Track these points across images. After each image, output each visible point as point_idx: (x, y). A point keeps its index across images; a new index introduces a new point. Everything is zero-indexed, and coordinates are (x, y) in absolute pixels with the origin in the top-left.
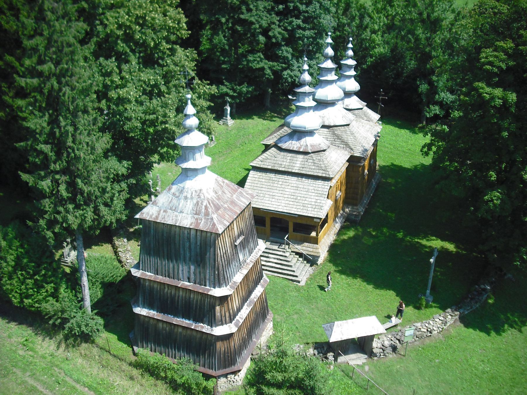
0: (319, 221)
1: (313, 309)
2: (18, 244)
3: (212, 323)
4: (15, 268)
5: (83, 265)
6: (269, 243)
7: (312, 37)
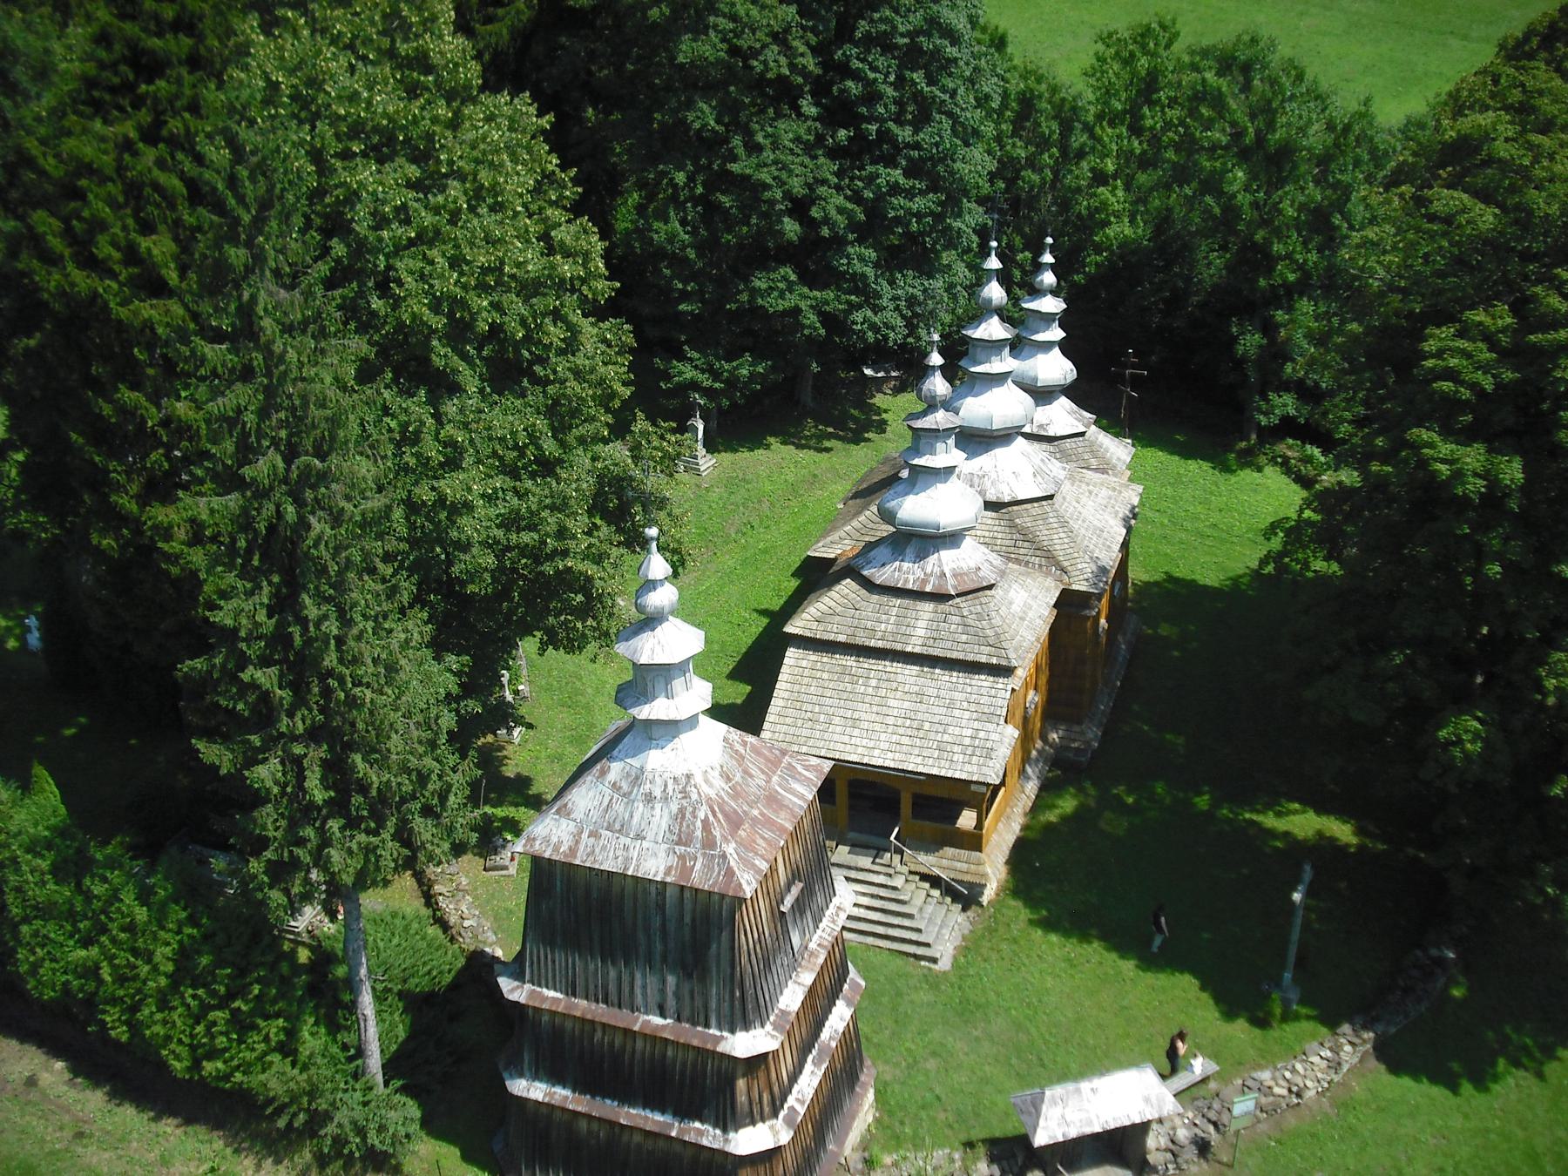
0: (984, 789)
1: (977, 1039)
2: (183, 915)
3: (728, 1119)
4: (176, 980)
5: (360, 964)
6: (847, 849)
7: (932, 213)
